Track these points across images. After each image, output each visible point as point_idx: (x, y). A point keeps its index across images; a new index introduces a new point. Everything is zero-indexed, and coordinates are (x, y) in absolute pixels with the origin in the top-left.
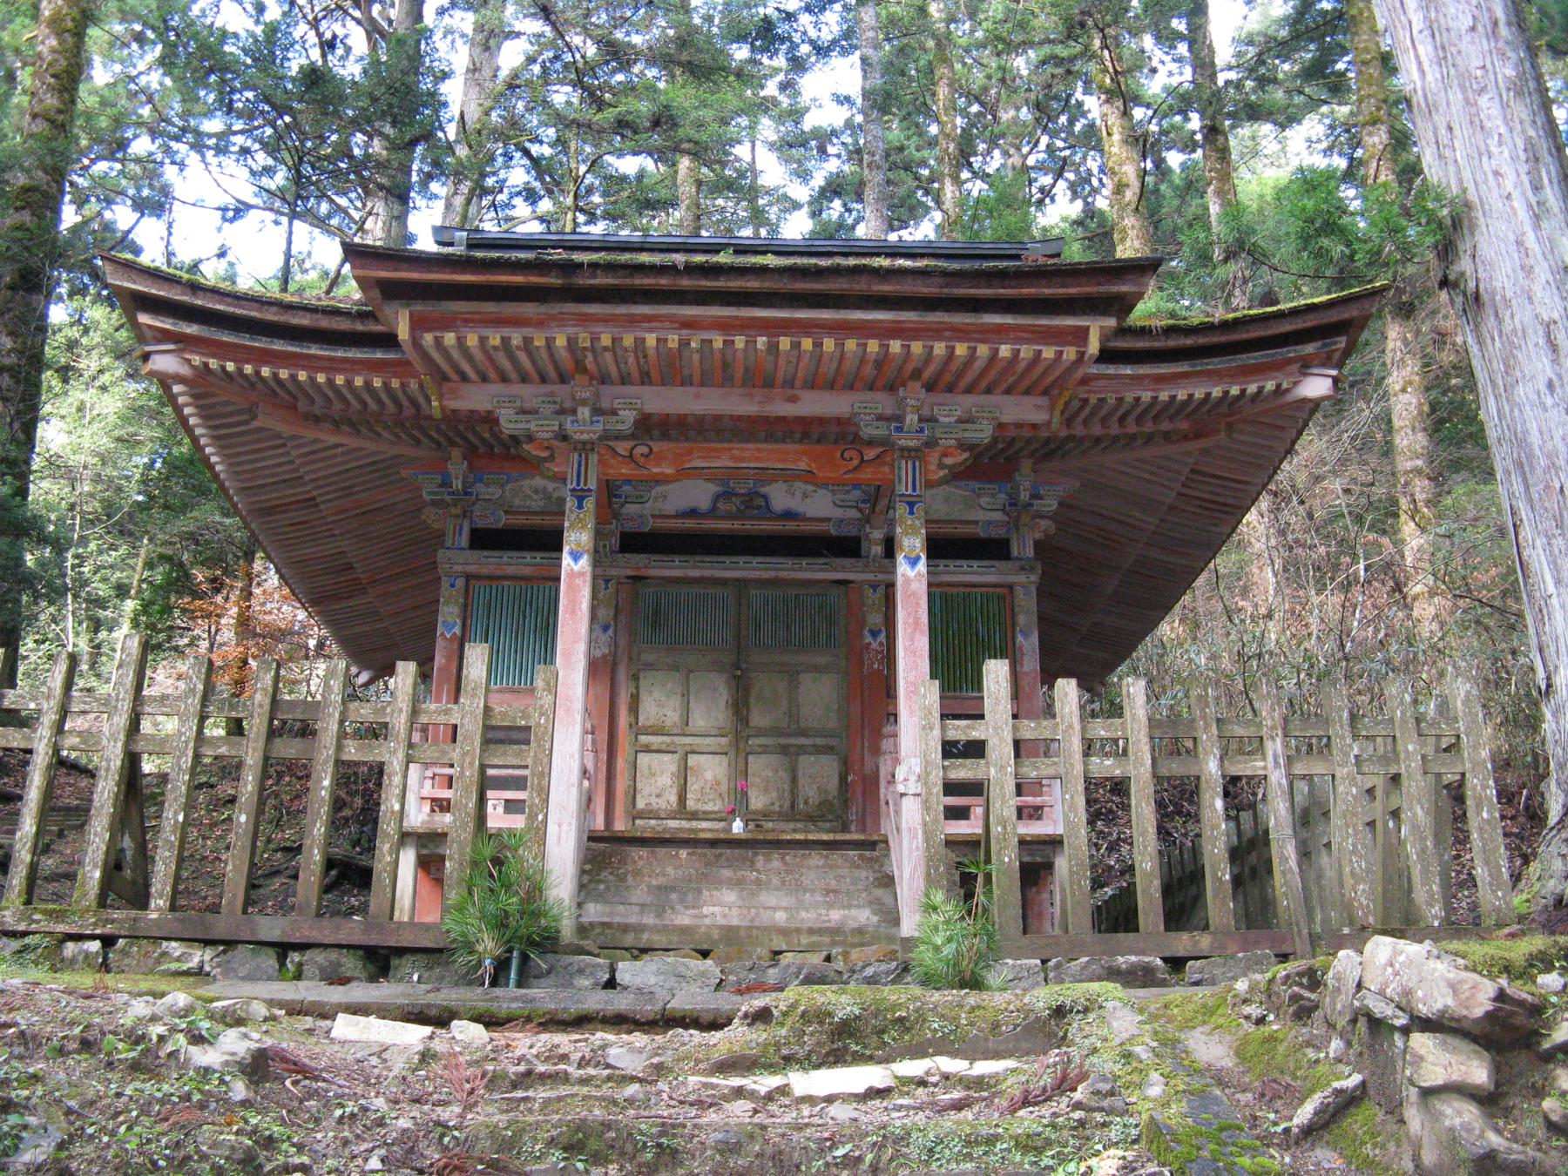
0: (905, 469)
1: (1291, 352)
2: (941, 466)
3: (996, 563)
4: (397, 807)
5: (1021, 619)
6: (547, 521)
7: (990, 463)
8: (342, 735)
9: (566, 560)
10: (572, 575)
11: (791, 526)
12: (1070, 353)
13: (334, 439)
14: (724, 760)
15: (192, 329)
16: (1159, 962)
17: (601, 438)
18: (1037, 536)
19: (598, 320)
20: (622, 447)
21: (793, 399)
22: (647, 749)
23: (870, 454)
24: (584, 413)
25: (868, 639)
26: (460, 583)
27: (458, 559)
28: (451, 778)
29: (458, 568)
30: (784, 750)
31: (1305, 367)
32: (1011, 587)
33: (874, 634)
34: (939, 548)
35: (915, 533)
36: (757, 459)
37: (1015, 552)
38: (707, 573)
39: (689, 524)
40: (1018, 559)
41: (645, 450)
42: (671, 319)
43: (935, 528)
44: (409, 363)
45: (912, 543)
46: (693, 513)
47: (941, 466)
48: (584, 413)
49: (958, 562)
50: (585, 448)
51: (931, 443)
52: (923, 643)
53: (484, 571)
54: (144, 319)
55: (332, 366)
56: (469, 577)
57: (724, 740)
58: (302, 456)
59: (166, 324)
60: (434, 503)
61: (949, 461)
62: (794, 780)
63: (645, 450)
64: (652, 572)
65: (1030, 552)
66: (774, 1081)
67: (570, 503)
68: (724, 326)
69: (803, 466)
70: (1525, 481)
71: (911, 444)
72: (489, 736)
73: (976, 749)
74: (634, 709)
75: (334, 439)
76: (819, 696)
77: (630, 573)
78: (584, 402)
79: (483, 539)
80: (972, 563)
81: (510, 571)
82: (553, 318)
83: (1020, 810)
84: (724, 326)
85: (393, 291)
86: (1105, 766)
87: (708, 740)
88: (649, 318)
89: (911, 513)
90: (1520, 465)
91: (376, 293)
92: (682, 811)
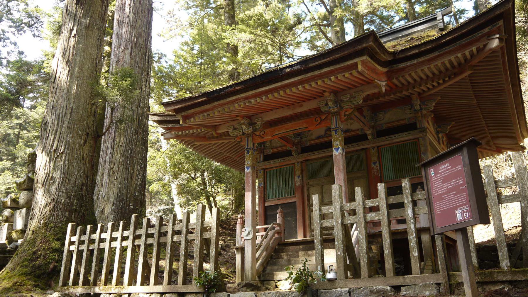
0: (333, 119)
1: (479, 34)
2: (345, 115)
3: (411, 132)
8: (173, 235)
9: (246, 170)
10: (247, 173)
16: (389, 288)
19: (225, 104)
21: (301, 106)
23: (323, 117)
25: (373, 165)
26: (262, 171)
29: (261, 168)
31: (489, 36)
32: (418, 139)
33: (375, 163)
34: (348, 141)
36: (292, 128)
37: (418, 126)
38: (324, 155)
39: (319, 141)
40: (420, 128)
41: (263, 132)
42: (241, 98)
43: (347, 134)
46: (319, 137)
49: (399, 134)
53: (267, 167)
56: (264, 170)
58: (467, 86)
61: (347, 113)
63: (263, 132)
68: (255, 96)
71: (335, 110)
75: (221, 142)
80: (403, 134)
81: (273, 166)
84: (255, 96)
86: (371, 216)
89: (336, 133)
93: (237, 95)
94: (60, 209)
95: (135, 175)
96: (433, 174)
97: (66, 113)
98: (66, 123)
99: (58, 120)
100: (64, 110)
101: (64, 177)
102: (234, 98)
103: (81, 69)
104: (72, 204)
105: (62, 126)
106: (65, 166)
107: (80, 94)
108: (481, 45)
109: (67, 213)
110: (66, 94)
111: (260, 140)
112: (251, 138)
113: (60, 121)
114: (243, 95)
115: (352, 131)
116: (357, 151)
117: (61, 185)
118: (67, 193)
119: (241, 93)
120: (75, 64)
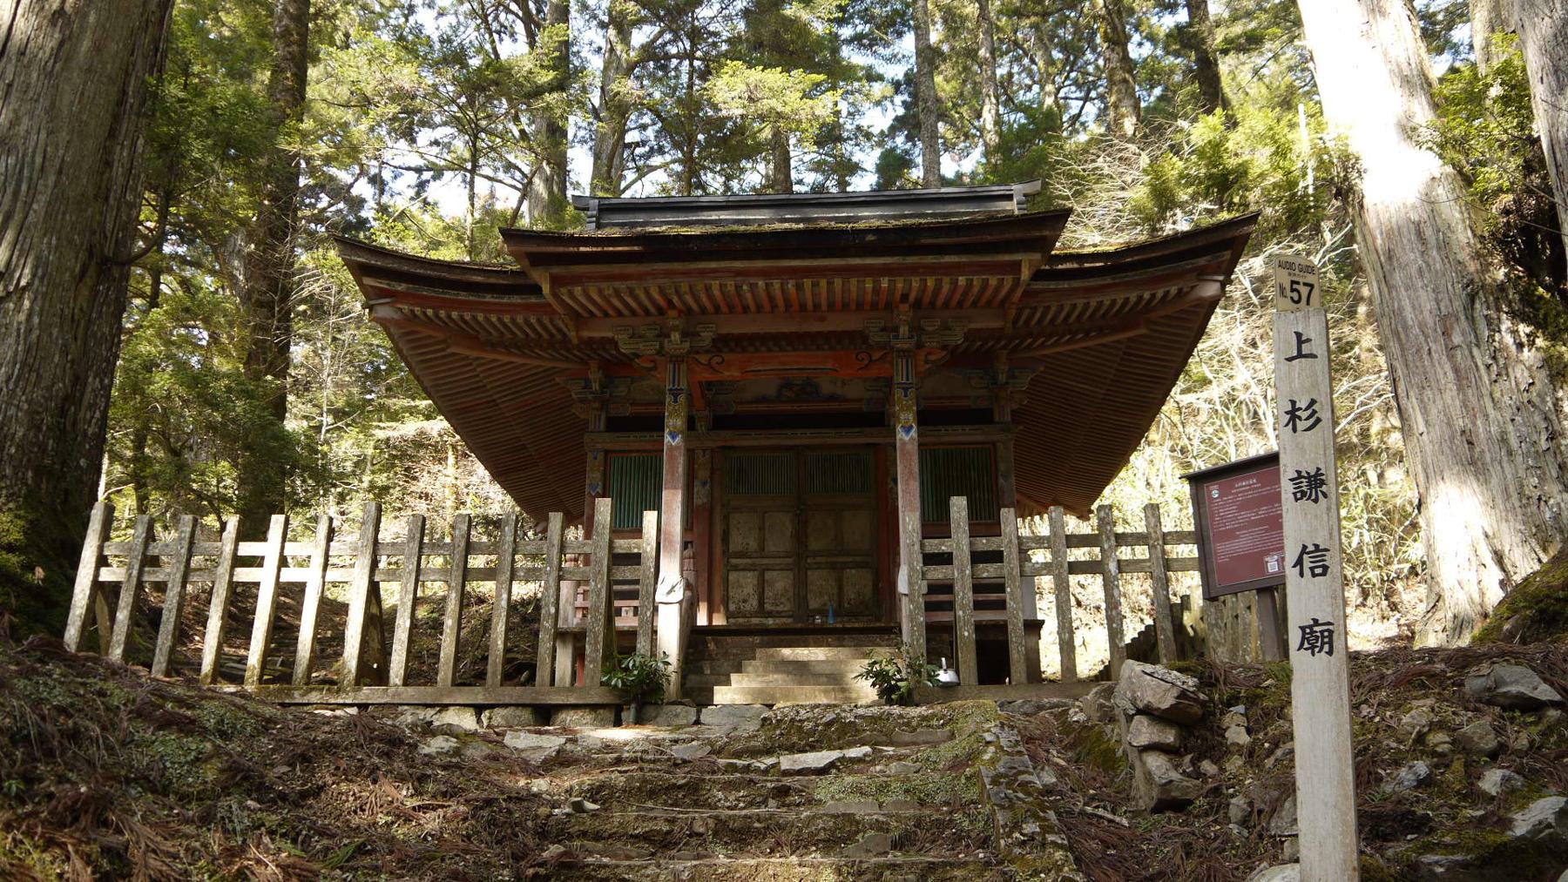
0: (901, 365)
1: (1188, 264)
2: (926, 362)
4: (553, 610)
5: (1002, 467)
6: (653, 409)
7: (974, 356)
9: (667, 438)
10: (671, 448)
11: (835, 406)
12: (1008, 281)
13: (506, 359)
14: (790, 574)
15: (401, 287)
17: (689, 352)
18: (1015, 407)
20: (703, 359)
21: (822, 319)
22: (736, 568)
23: (876, 356)
24: (675, 336)
26: (601, 456)
27: (599, 441)
28: (636, 608)
30: (832, 566)
32: (994, 444)
35: (908, 408)
39: (762, 407)
41: (719, 360)
42: (728, 270)
44: (549, 305)
45: (908, 417)
46: (763, 399)
47: (926, 362)
48: (675, 336)
50: (677, 360)
51: (919, 346)
52: (915, 486)
53: (618, 447)
54: (368, 281)
55: (501, 309)
56: (607, 452)
57: (790, 560)
59: (383, 285)
60: (581, 401)
61: (932, 358)
62: (840, 588)
63: (719, 360)
64: (735, 443)
65: (1008, 418)
66: (770, 761)
67: (669, 399)
68: (765, 274)
69: (829, 366)
70: (1401, 345)
71: (905, 347)
72: (981, 597)
73: (946, 559)
74: (726, 539)
75: (506, 359)
76: (857, 528)
77: (720, 444)
78: (675, 328)
79: (615, 425)
81: (635, 446)
82: (648, 274)
83: (976, 603)
84: (765, 274)
85: (536, 260)
87: (778, 561)
88: (715, 271)
90: (1396, 334)
91: (526, 263)
92: (761, 611)
93: (723, 259)
94: (11, 457)
95: (85, 403)
96: (1215, 494)
97: (42, 169)
98: (43, 199)
99: (18, 186)
100: (38, 160)
101: (24, 364)
102: (713, 265)
103: (97, 48)
104: (43, 449)
105: (28, 206)
106: (29, 331)
107: (87, 124)
108: (1184, 284)
109: (30, 474)
110: (47, 112)
111: (707, 376)
112: (684, 367)
113: (24, 187)
114: (738, 264)
115: (847, 401)
116: (855, 446)
117: (16, 385)
118: (32, 413)
119: (735, 259)
120: (82, 29)
